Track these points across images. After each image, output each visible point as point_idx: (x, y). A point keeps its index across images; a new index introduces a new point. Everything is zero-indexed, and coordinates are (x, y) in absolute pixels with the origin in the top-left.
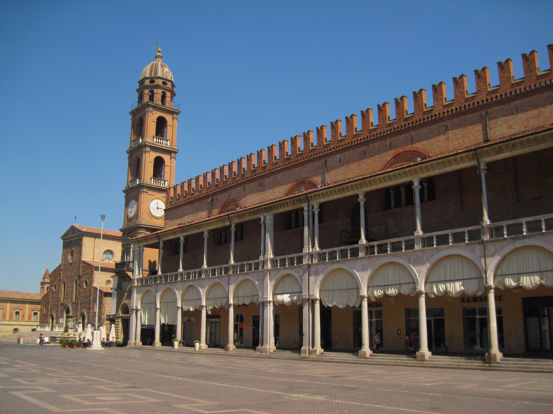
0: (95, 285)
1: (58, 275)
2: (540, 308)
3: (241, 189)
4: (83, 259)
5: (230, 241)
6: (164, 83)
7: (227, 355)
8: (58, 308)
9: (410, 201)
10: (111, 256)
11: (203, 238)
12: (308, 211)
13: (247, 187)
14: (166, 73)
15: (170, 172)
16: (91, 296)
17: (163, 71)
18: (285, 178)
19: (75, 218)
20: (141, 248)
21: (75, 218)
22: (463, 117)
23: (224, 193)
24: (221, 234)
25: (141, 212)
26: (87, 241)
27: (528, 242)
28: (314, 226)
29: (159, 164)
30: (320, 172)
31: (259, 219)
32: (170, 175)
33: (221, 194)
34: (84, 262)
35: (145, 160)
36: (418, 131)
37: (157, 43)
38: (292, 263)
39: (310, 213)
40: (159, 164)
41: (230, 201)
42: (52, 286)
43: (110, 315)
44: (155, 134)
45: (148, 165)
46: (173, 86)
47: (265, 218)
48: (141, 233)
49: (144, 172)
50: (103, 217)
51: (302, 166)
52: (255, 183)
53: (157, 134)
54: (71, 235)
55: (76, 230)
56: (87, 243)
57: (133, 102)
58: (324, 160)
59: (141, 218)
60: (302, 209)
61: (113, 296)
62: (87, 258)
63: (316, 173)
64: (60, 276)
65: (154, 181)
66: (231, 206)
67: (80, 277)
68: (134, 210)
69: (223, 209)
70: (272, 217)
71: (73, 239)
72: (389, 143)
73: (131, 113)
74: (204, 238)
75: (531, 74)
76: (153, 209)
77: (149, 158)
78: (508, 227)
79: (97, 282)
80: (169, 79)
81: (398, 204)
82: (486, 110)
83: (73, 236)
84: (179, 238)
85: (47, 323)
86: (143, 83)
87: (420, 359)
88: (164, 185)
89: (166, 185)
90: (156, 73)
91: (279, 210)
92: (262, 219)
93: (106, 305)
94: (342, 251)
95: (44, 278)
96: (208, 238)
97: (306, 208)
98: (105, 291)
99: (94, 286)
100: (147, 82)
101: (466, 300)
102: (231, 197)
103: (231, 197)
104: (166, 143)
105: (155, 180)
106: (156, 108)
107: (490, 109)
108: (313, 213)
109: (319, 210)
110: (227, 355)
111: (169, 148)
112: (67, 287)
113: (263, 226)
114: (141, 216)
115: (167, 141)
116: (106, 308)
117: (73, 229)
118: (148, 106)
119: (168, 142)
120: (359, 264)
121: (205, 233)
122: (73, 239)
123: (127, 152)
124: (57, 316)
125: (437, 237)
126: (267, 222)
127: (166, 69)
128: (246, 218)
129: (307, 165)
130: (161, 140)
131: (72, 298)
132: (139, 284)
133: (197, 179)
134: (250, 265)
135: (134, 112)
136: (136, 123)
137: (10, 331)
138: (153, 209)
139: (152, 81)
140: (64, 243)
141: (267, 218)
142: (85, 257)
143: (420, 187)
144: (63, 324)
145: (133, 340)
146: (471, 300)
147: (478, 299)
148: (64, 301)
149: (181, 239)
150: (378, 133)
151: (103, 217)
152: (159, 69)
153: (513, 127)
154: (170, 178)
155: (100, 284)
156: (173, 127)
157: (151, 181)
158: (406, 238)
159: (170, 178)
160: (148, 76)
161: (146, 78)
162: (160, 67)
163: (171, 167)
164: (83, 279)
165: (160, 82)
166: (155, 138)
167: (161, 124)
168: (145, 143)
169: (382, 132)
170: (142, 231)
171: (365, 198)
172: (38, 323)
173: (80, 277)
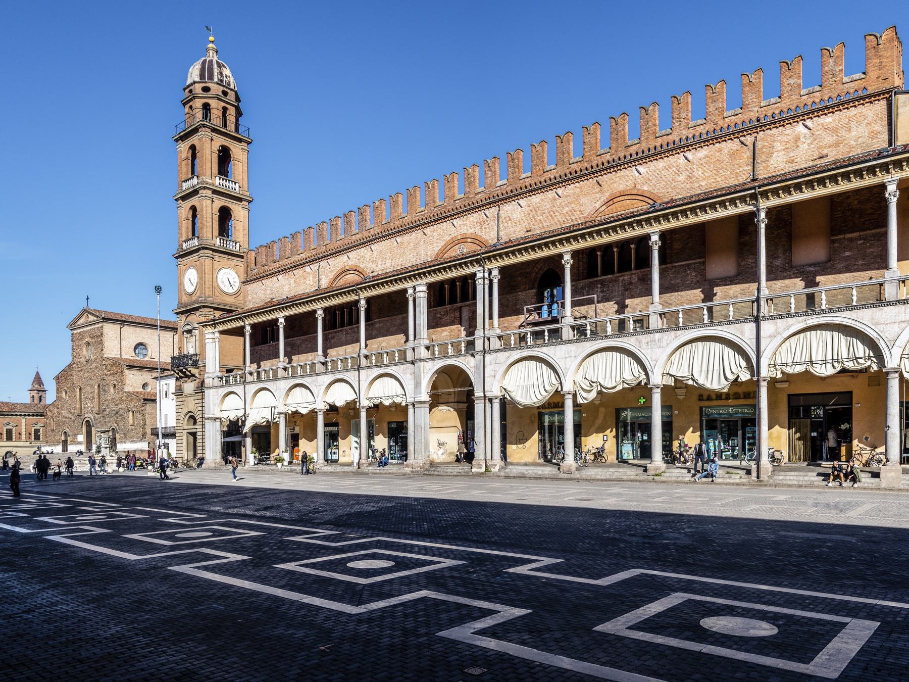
2: (813, 408)
5: (358, 322)
7: (572, 479)
9: (644, 262)
11: (316, 319)
18: (435, 234)
19: (88, 299)
21: (88, 299)
24: (335, 315)
28: (492, 299)
29: (225, 215)
37: (207, 27)
39: (487, 281)
40: (225, 215)
44: (217, 172)
46: (238, 99)
50: (158, 289)
52: (731, 146)
53: (220, 173)
58: (315, 267)
63: (483, 227)
70: (424, 288)
75: (834, 79)
77: (209, 208)
78: (549, 331)
79: (131, 384)
80: (232, 87)
81: (453, 300)
84: (276, 320)
87: (653, 473)
88: (234, 248)
92: (410, 291)
96: (285, 327)
101: (705, 398)
108: (491, 281)
110: (572, 479)
115: (235, 183)
119: (237, 184)
125: (549, 331)
127: (227, 72)
132: (234, 383)
142: (108, 352)
146: (714, 397)
147: (724, 397)
150: (582, 168)
151: (158, 289)
153: (796, 161)
162: (215, 66)
167: (224, 157)
169: (616, 159)
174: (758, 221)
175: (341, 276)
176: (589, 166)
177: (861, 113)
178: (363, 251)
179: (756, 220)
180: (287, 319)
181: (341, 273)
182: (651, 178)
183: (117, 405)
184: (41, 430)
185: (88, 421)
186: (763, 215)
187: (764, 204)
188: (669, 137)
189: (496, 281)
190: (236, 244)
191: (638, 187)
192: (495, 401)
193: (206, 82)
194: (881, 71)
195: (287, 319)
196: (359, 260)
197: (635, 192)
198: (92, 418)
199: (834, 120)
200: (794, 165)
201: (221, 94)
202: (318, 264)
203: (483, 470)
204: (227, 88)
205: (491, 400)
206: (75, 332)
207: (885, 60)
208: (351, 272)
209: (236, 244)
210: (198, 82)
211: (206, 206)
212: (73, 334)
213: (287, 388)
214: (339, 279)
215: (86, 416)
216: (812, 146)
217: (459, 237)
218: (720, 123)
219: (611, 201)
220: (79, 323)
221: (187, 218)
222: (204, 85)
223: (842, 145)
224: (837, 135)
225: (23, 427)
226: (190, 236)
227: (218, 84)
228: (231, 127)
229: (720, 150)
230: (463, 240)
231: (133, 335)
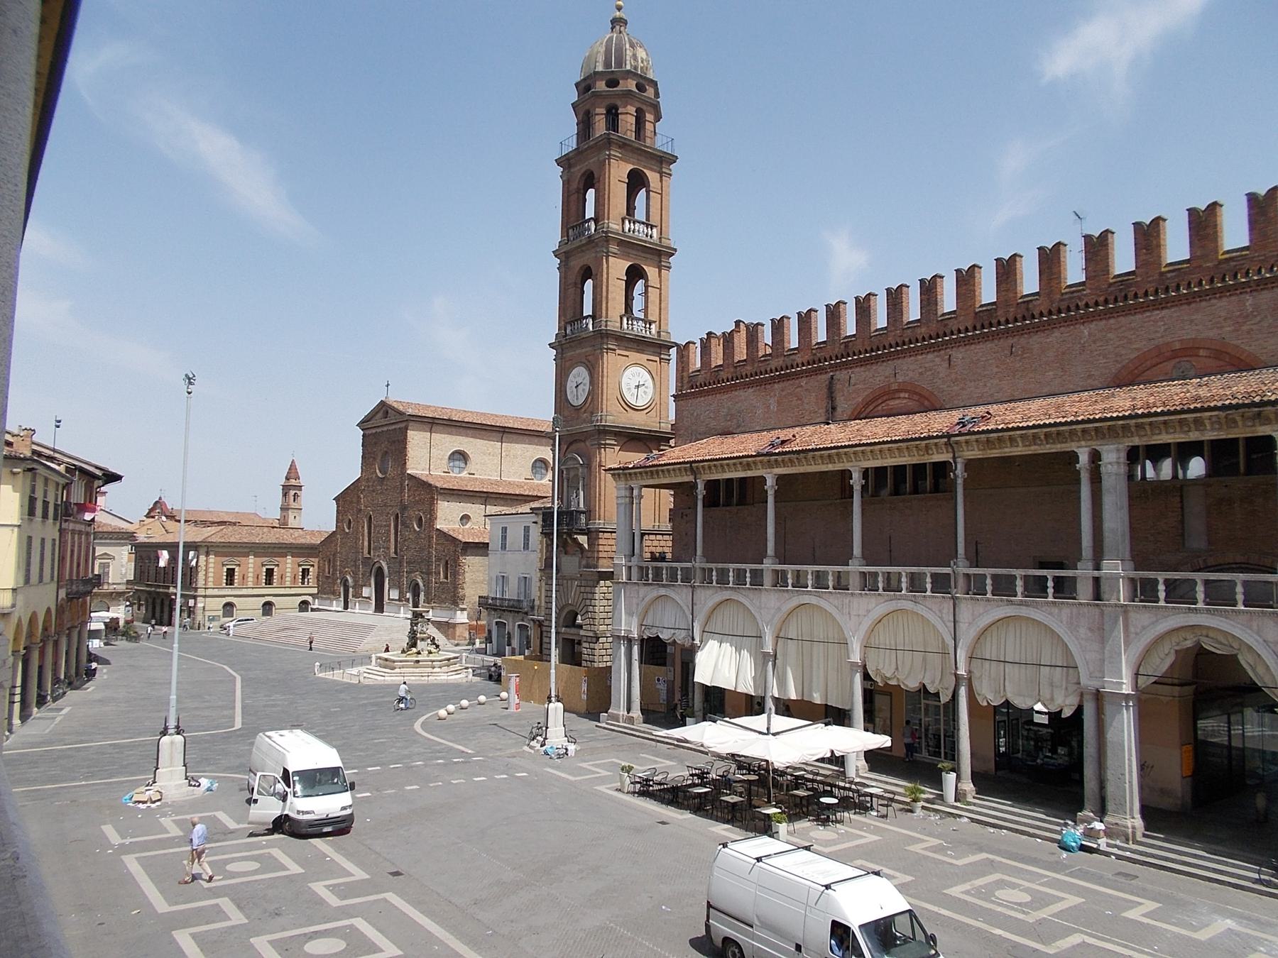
0: (695, 680)
1: (354, 500)
4: (408, 472)
6: (641, 88)
8: (357, 567)
10: (462, 465)
13: (960, 356)
14: (642, 62)
15: (660, 300)
16: (430, 546)
17: (635, 57)
19: (388, 385)
20: (636, 493)
21: (388, 385)
23: (874, 367)
25: (605, 397)
26: (416, 439)
32: (660, 309)
33: (862, 369)
34: (411, 477)
35: (608, 274)
38: (673, 577)
41: (895, 387)
42: (342, 520)
43: (487, 598)
45: (614, 285)
48: (605, 444)
49: (607, 303)
51: (1185, 307)
54: (379, 420)
55: (390, 411)
56: (416, 438)
57: (565, 134)
59: (604, 410)
61: (490, 556)
62: (417, 470)
63: (1245, 328)
64: (358, 502)
65: (628, 324)
66: (897, 402)
67: (404, 508)
68: (584, 390)
69: (871, 407)
71: (385, 429)
73: (559, 162)
74: (852, 487)
76: (629, 389)
83: (384, 422)
85: (335, 594)
86: (588, 88)
89: (653, 331)
90: (620, 62)
91: (1155, 437)
93: (467, 568)
95: (287, 479)
98: (464, 540)
99: (438, 527)
100: (601, 86)
104: (650, 232)
105: (630, 322)
106: (624, 145)
111: (656, 245)
112: (375, 527)
114: (604, 407)
116: (467, 575)
117: (384, 409)
118: (607, 142)
119: (654, 230)
122: (385, 429)
123: (556, 254)
124: (355, 581)
128: (1015, 449)
129: (1204, 304)
130: (630, 223)
131: (388, 548)
133: (778, 326)
135: (568, 159)
137: (256, 607)
138: (629, 389)
139: (613, 83)
140: (364, 436)
144: (369, 598)
145: (622, 709)
148: (369, 553)
152: (628, 52)
154: (660, 314)
155: (449, 522)
156: (661, 194)
157: (621, 324)
159: (660, 314)
160: (600, 68)
161: (595, 75)
163: (660, 289)
164: (413, 513)
165: (631, 85)
166: (627, 222)
168: (606, 232)
170: (608, 442)
172: (315, 591)
173: (404, 508)
175: (880, 401)
181: (880, 396)
184: (311, 570)
196: (921, 374)
206: (368, 432)
208: (902, 395)
214: (874, 405)
217: (1177, 346)
231: (450, 442)
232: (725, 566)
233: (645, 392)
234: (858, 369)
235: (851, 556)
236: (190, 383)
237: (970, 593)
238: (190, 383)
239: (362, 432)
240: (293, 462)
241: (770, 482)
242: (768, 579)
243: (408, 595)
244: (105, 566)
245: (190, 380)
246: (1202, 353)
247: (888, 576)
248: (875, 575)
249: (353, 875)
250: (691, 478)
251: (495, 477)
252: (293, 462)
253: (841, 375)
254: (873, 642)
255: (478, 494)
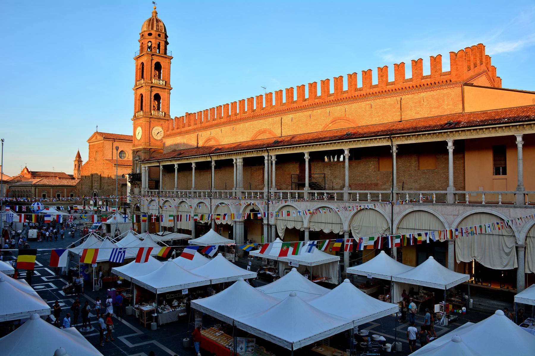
3: (219, 130)
12: (268, 160)
18: (251, 126)
19: (97, 127)
21: (97, 127)
22: (384, 99)
23: (207, 131)
27: (422, 208)
30: (277, 126)
31: (232, 160)
36: (350, 105)
39: (270, 161)
47: (236, 159)
58: (278, 118)
60: (263, 157)
70: (241, 160)
72: (328, 111)
82: (401, 96)
92: (235, 161)
94: (291, 193)
97: (266, 158)
102: (212, 135)
103: (212, 135)
107: (404, 96)
108: (272, 162)
109: (397, 151)
113: (235, 165)
120: (342, 205)
121: (193, 165)
126: (238, 164)
134: (256, 193)
136: (139, 67)
141: (238, 161)
143: (523, 142)
149: (176, 166)
158: (189, 191)
171: (453, 146)
174: (392, 152)
176: (324, 102)
177: (449, 92)
178: (218, 130)
179: (391, 151)
180: (179, 165)
182: (353, 112)
183: (109, 186)
185: (95, 193)
186: (394, 149)
187: (215, 158)
188: (361, 92)
189: (274, 162)
190: (162, 113)
191: (347, 116)
192: (272, 227)
193: (150, 31)
194: (458, 72)
195: (179, 165)
197: (345, 119)
198: (97, 191)
199: (437, 94)
200: (419, 115)
201: (157, 36)
202: (280, 118)
203: (266, 263)
204: (160, 32)
205: (271, 226)
206: (91, 144)
207: (459, 67)
209: (162, 113)
210: (147, 31)
211: (148, 95)
212: (89, 145)
213: (178, 203)
215: (95, 190)
216: (427, 106)
217: (263, 130)
218: (385, 88)
219: (333, 121)
220: (92, 140)
221: (139, 100)
222: (149, 32)
223: (440, 108)
224: (438, 102)
225: (65, 193)
226: (140, 110)
227: (156, 31)
228: (162, 51)
229: (385, 102)
230: (264, 132)
232: (200, 191)
233: (161, 135)
234: (203, 132)
235: (174, 187)
236: (3, 142)
237: (351, 200)
238: (3, 142)
239: (89, 144)
240: (79, 152)
241: (176, 166)
242: (346, 197)
243: (105, 203)
244: (33, 208)
245: (2, 140)
246: (267, 132)
247: (291, 193)
248: (367, 194)
249: (125, 338)
250: (158, 164)
251: (458, 109)
252: (79, 152)
253: (200, 133)
254: (312, 220)
255: (129, 167)
